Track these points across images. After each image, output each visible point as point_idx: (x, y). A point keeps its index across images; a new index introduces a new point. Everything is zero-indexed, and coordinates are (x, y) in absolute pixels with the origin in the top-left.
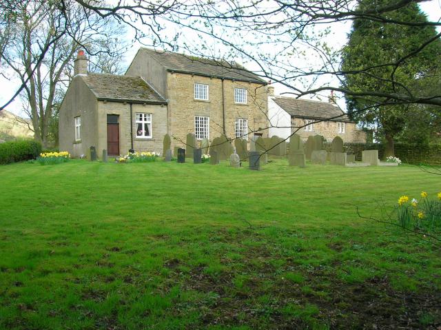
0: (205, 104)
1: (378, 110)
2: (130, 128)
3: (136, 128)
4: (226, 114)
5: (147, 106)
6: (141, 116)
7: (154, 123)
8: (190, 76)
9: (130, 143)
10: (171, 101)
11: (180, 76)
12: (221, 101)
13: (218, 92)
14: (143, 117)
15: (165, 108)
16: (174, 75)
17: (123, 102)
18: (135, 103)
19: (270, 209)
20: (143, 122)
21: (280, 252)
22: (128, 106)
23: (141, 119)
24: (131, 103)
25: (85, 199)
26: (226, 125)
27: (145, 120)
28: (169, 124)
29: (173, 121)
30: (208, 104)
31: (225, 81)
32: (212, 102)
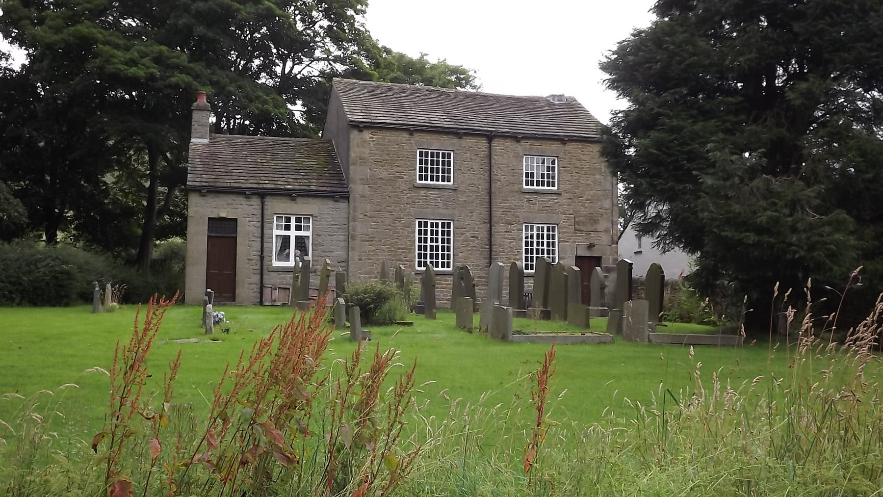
0: (446, 193)
1: (836, 103)
2: (259, 244)
3: (275, 246)
4: (497, 213)
5: (299, 200)
6: (288, 220)
7: (316, 234)
8: (405, 136)
9: (259, 277)
10: (357, 189)
11: (380, 135)
12: (483, 186)
13: (478, 166)
14: (293, 223)
15: (343, 205)
16: (367, 135)
17: (244, 194)
18: (272, 195)
19: (124, 350)
20: (293, 233)
21: (23, 490)
22: (256, 202)
23: (288, 228)
24: (262, 194)
25: (122, 376)
26: (497, 239)
27: (298, 228)
28: (350, 237)
29: (360, 228)
30: (452, 193)
31: (496, 143)
32: (462, 188)
